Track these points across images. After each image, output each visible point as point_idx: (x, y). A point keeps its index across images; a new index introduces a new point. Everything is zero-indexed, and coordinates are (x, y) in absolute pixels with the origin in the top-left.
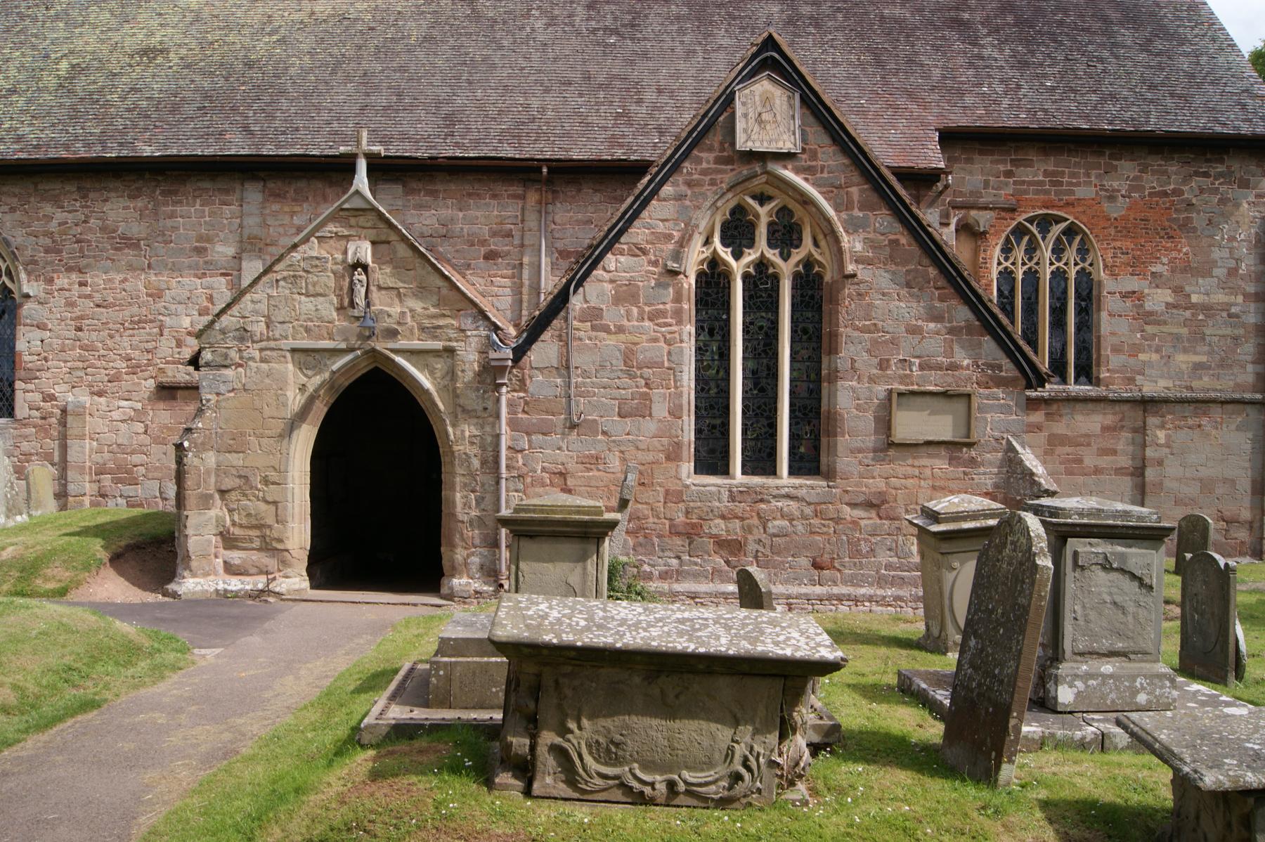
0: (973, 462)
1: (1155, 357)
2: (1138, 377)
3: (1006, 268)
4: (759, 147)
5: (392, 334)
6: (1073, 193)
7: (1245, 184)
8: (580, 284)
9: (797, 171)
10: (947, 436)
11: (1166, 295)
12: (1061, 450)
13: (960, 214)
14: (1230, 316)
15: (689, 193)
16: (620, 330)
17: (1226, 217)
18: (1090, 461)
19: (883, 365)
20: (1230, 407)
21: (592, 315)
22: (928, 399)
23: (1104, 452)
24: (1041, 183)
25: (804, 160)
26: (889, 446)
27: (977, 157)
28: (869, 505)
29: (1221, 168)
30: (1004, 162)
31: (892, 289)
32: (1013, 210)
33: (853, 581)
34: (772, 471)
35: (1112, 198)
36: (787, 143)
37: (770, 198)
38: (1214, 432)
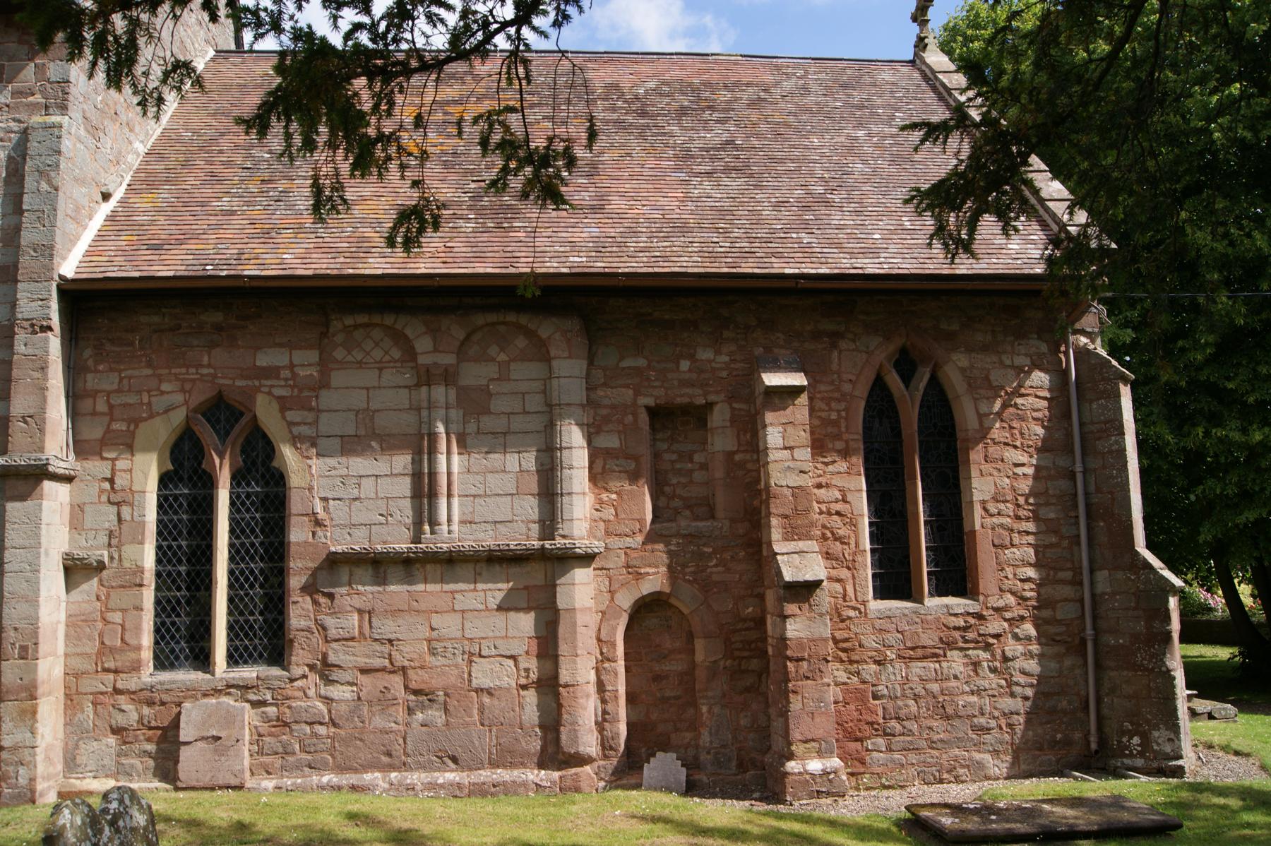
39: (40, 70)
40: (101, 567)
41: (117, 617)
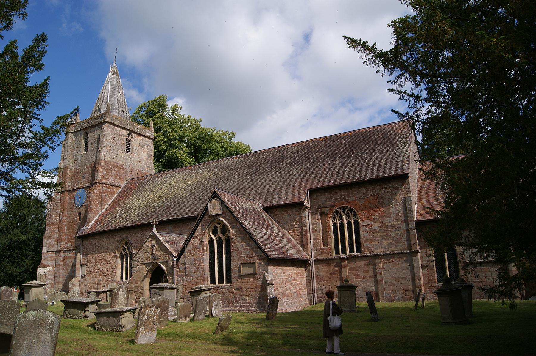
0: (257, 278)
1: (377, 242)
4: (213, 214)
5: (159, 259)
8: (187, 246)
9: (222, 217)
10: (252, 273)
11: (378, 224)
12: (353, 272)
13: (320, 210)
17: (393, 199)
18: (362, 275)
19: (240, 257)
20: (401, 255)
24: (340, 198)
25: (224, 215)
26: (241, 276)
27: (323, 194)
28: (238, 289)
29: (390, 185)
31: (240, 240)
33: (236, 307)
35: (360, 199)
36: (220, 212)
39: (405, 187)
40: (427, 266)
41: (431, 274)
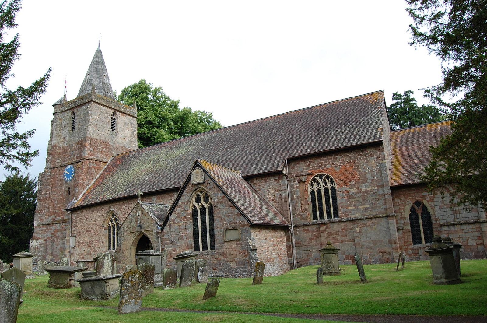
1: (354, 208)
2: (350, 214)
3: (319, 189)
6: (326, 167)
7: (372, 155)
13: (298, 178)
14: (374, 193)
15: (10, 225)
16: (178, 223)
18: (339, 239)
19: (223, 224)
21: (174, 220)
22: (231, 230)
23: (343, 236)
27: (301, 163)
29: (365, 152)
30: (307, 163)
32: (311, 174)
34: (420, 242)
35: (336, 166)
37: (203, 192)
38: (374, 227)
